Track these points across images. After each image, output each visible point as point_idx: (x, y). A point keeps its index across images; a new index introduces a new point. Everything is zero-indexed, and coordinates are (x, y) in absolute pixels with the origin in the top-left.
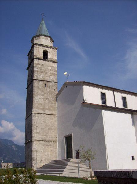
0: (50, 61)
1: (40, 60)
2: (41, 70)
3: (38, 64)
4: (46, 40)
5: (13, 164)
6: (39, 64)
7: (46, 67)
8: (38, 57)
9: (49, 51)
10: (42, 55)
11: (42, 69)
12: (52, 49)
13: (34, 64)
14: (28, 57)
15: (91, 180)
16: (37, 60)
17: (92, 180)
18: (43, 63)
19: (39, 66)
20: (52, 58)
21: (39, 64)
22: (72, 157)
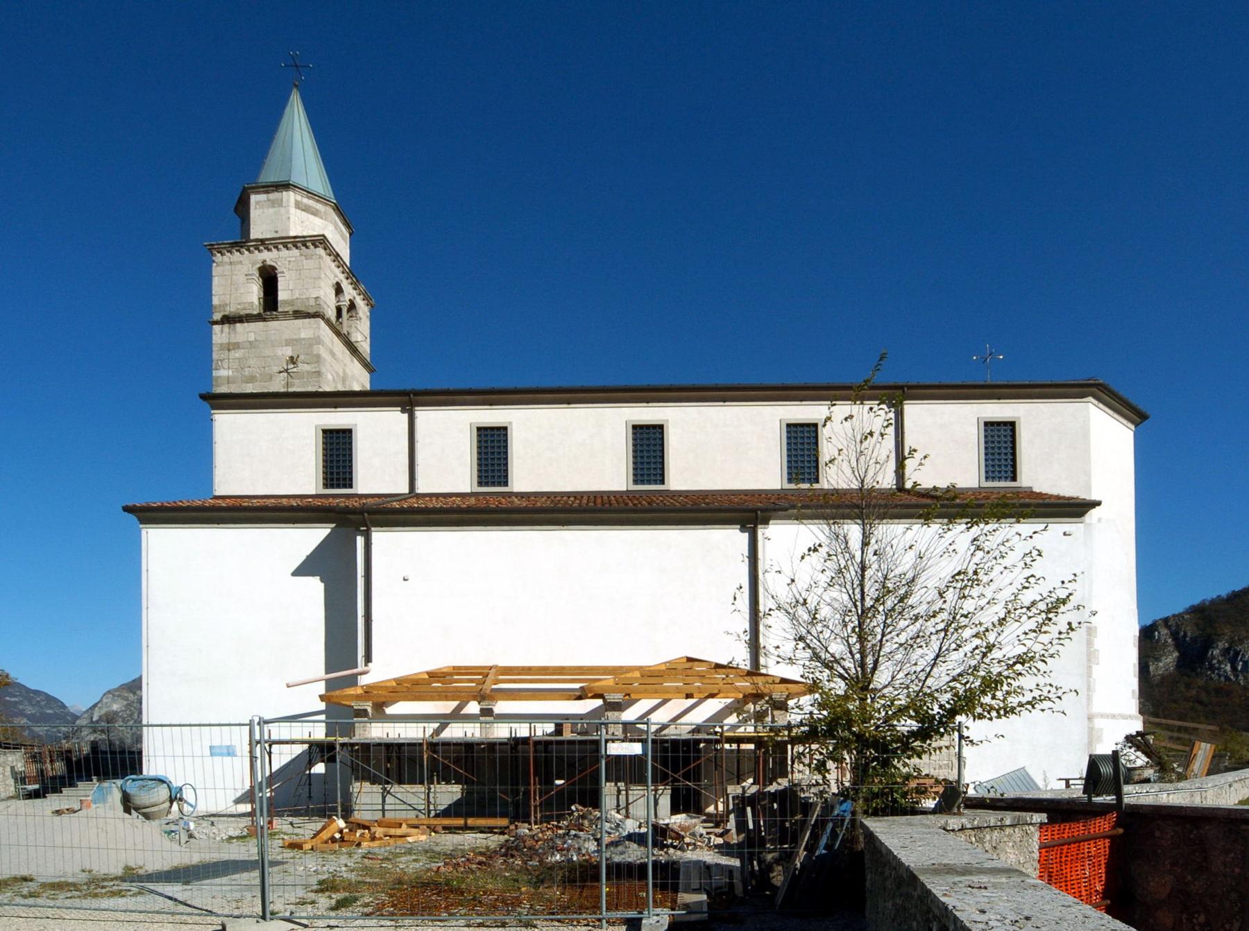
0: (298, 315)
1: (238, 325)
2: (247, 372)
3: (230, 347)
4: (271, 210)
5: (357, 779)
6: (237, 346)
7: (268, 352)
8: (232, 309)
9: (281, 267)
10: (253, 294)
11: (252, 362)
12: (295, 252)
13: (215, 348)
14: (932, 487)
15: (812, 743)
16: (226, 326)
17: (739, 750)
18: (252, 337)
19: (237, 354)
20: (297, 295)
21: (237, 346)
22: (491, 709)
